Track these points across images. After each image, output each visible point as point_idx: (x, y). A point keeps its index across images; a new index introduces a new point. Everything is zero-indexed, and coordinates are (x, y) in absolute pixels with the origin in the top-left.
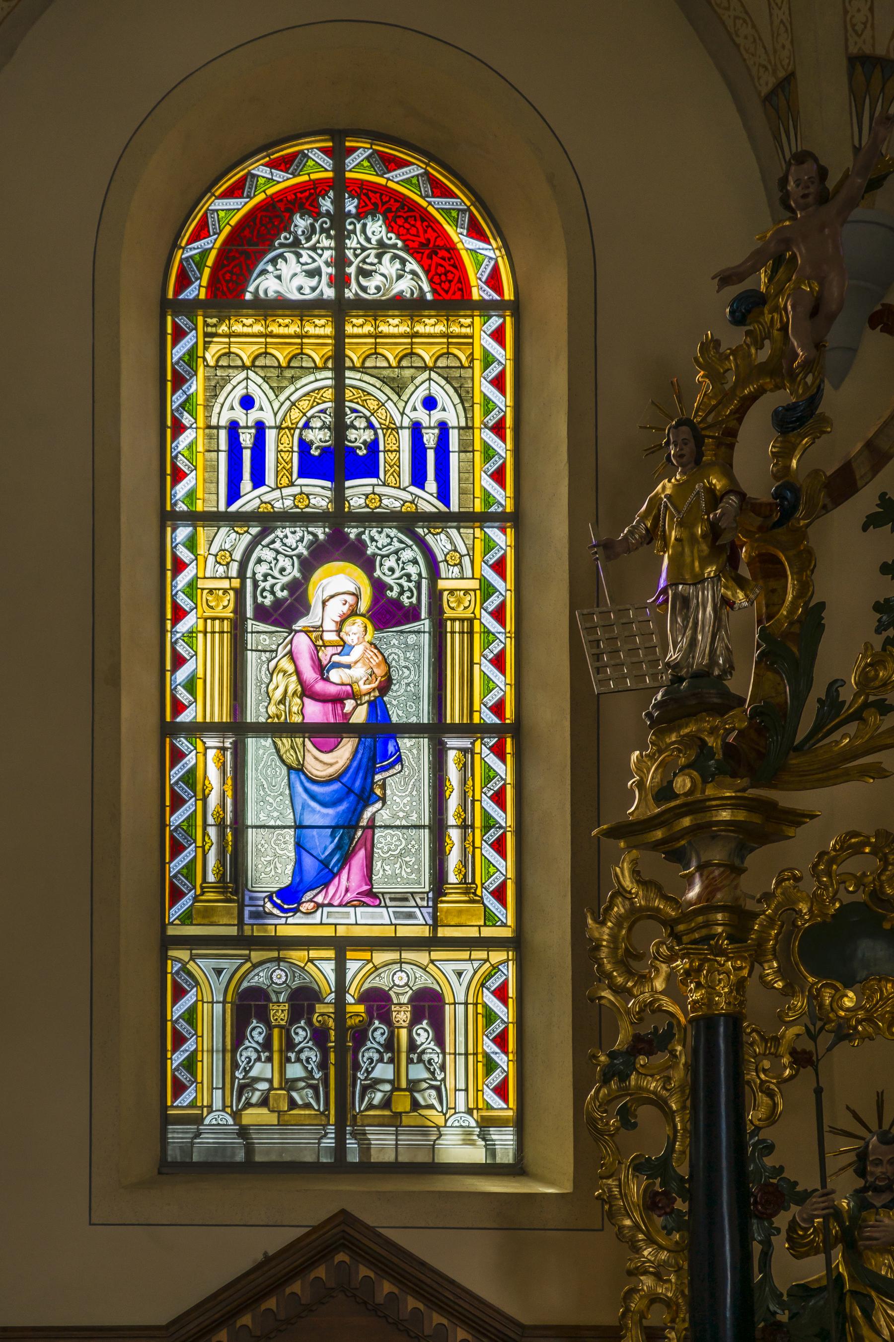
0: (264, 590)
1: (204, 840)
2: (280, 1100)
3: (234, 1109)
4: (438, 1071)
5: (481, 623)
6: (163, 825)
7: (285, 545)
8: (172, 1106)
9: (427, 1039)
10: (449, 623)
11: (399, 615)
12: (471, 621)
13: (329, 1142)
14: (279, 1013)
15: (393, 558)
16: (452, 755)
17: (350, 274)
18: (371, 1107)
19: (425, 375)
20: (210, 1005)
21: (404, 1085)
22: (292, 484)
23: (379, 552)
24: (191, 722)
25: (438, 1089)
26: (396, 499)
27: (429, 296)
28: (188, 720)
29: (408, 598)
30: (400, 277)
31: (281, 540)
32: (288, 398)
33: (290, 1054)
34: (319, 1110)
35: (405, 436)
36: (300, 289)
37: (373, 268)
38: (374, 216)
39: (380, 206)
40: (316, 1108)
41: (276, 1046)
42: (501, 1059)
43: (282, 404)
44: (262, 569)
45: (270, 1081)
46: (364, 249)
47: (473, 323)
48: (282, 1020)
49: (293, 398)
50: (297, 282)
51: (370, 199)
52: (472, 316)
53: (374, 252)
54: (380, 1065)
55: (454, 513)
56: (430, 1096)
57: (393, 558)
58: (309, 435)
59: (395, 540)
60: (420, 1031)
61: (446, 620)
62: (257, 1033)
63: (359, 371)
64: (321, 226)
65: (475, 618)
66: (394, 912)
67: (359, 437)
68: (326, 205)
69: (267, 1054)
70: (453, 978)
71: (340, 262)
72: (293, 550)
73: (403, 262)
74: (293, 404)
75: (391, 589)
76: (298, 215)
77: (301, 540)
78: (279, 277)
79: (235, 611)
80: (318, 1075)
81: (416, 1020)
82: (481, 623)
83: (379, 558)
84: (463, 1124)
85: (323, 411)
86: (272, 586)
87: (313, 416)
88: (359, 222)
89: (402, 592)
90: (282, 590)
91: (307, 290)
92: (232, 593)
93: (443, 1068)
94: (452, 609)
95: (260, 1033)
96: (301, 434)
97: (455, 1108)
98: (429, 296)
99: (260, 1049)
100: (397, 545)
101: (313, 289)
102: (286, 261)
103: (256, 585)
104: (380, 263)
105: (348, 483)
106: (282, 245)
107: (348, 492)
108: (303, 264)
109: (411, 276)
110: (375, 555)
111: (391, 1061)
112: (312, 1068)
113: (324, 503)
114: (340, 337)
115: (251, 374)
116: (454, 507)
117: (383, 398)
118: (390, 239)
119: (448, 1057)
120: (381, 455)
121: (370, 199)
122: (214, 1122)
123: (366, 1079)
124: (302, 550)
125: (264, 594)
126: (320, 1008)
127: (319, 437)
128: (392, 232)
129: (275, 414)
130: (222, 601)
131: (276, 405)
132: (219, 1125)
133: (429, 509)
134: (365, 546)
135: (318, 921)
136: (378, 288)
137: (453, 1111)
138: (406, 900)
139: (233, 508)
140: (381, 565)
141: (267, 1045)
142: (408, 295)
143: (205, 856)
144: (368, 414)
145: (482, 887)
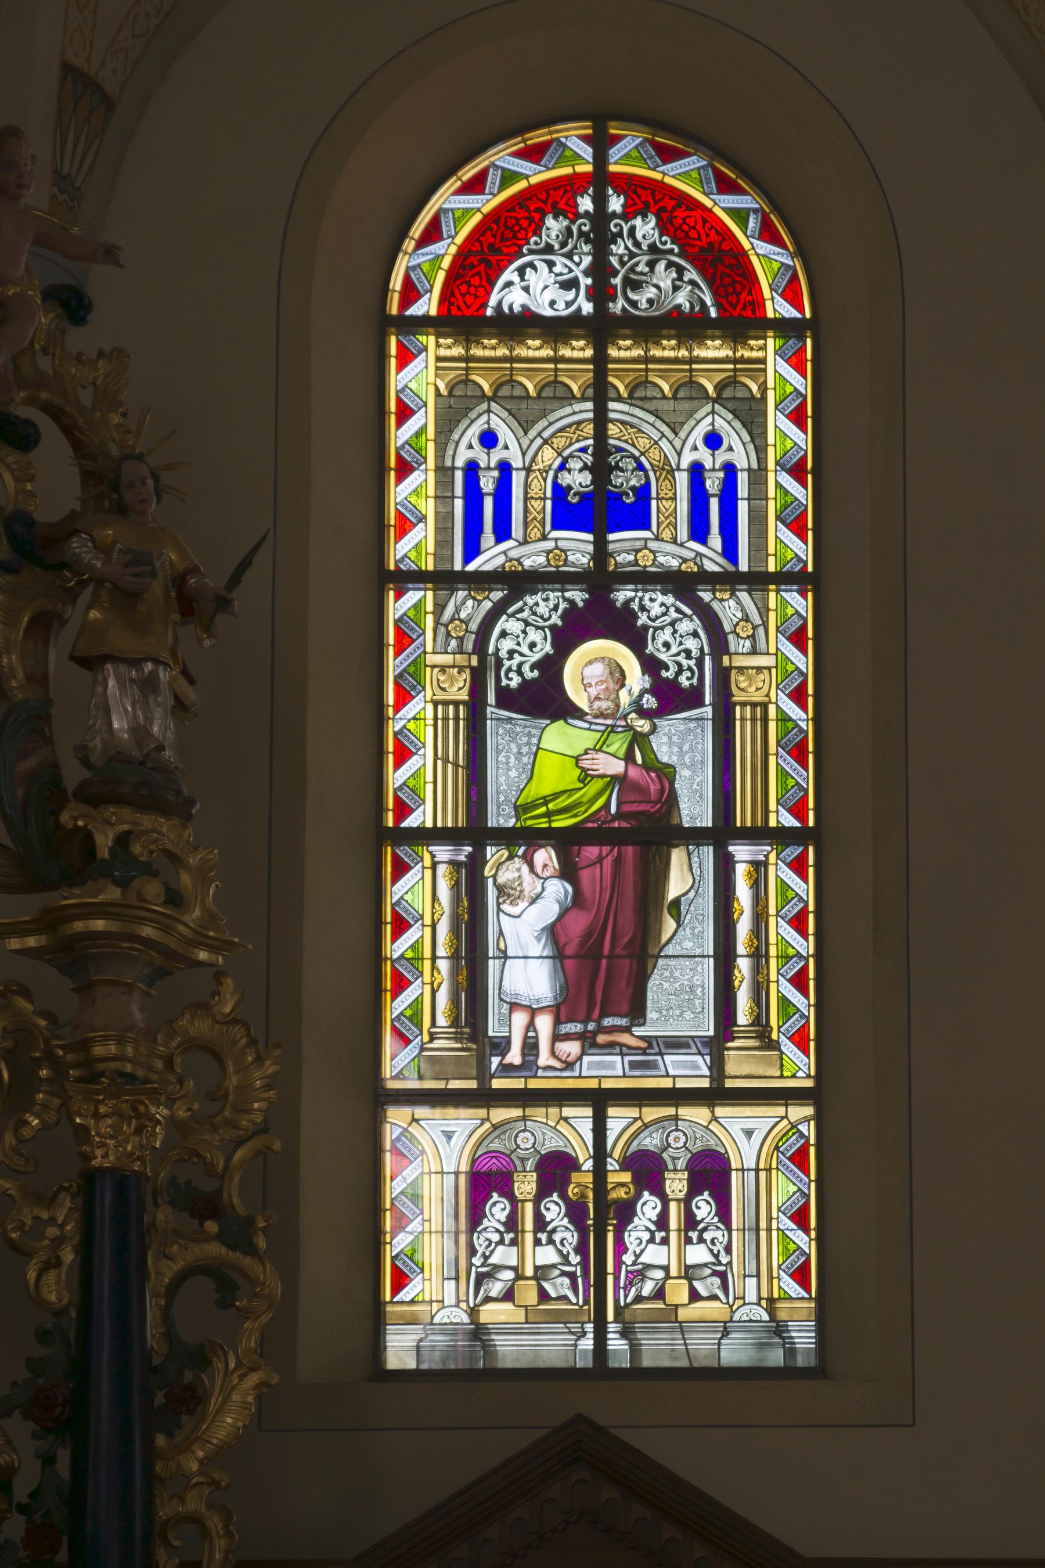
0: (509, 670)
1: (433, 975)
2: (528, 1294)
3: (472, 1305)
4: (723, 1253)
5: (778, 707)
6: (378, 958)
7: (535, 614)
8: (391, 1302)
9: (559, 1214)
10: (738, 708)
11: (678, 701)
12: (765, 706)
13: (588, 1343)
14: (526, 1185)
15: (669, 630)
16: (741, 871)
17: (616, 286)
18: (639, 1299)
19: (708, 408)
20: (440, 1176)
21: (529, 1272)
22: (544, 538)
23: (650, 623)
24: (418, 828)
25: (722, 1276)
26: (674, 556)
27: (713, 313)
28: (415, 825)
29: (688, 679)
30: (676, 289)
31: (531, 608)
32: (539, 435)
33: (690, 1234)
34: (577, 1304)
35: (682, 480)
36: (552, 303)
37: (643, 278)
38: (644, 216)
39: (544, 207)
40: (574, 1301)
41: (673, 1224)
42: (801, 1238)
43: (532, 442)
44: (507, 645)
45: (666, 1269)
46: (632, 255)
47: (765, 345)
48: (680, 1191)
49: (546, 434)
50: (548, 296)
51: (639, 197)
52: (765, 338)
53: (646, 258)
54: (500, 1248)
55: (743, 573)
56: (562, 1285)
57: (669, 630)
58: (565, 479)
59: (672, 610)
60: (551, 1205)
61: (735, 704)
62: (498, 1209)
63: (627, 403)
64: (579, 229)
65: (770, 702)
66: (630, 1062)
67: (625, 481)
68: (586, 204)
69: (511, 1235)
70: (741, 1138)
71: (600, 270)
72: (545, 620)
73: (680, 270)
74: (546, 442)
75: (667, 669)
76: (551, 215)
77: (556, 608)
78: (526, 289)
79: (472, 693)
80: (575, 1259)
81: (694, 1190)
82: (778, 707)
83: (651, 631)
84: (753, 1318)
85: (583, 450)
86: (520, 665)
87: (571, 456)
88: (626, 223)
89: (680, 671)
90: (532, 670)
91: (560, 305)
92: (468, 671)
93: (728, 1249)
94: (743, 690)
95: (504, 1209)
96: (556, 477)
97: (744, 1298)
98: (713, 313)
99: (502, 1229)
100: (674, 615)
101: (568, 304)
102: (536, 271)
103: (499, 663)
104: (652, 271)
105: (612, 537)
106: (531, 252)
107: (611, 547)
108: (557, 275)
109: (689, 288)
110: (645, 628)
111: (514, 1242)
112: (719, 1251)
113: (585, 560)
114: (600, 361)
115: (494, 406)
116: (744, 566)
117: (656, 434)
118: (665, 243)
119: (734, 1234)
120: (654, 503)
121: (639, 197)
122: (745, 1318)
123: (483, 1265)
124: (556, 620)
125: (511, 675)
126: (575, 1177)
127: (578, 480)
128: (667, 234)
129: (524, 454)
130: (457, 681)
131: (525, 443)
132: (751, 1321)
133: (716, 569)
134: (636, 617)
135: (577, 1074)
136: (650, 301)
137: (741, 1302)
138: (688, 1047)
139: (471, 567)
140: (654, 639)
141: (662, 1222)
142: (687, 310)
143: (434, 993)
144: (637, 454)
145: (779, 1031)
